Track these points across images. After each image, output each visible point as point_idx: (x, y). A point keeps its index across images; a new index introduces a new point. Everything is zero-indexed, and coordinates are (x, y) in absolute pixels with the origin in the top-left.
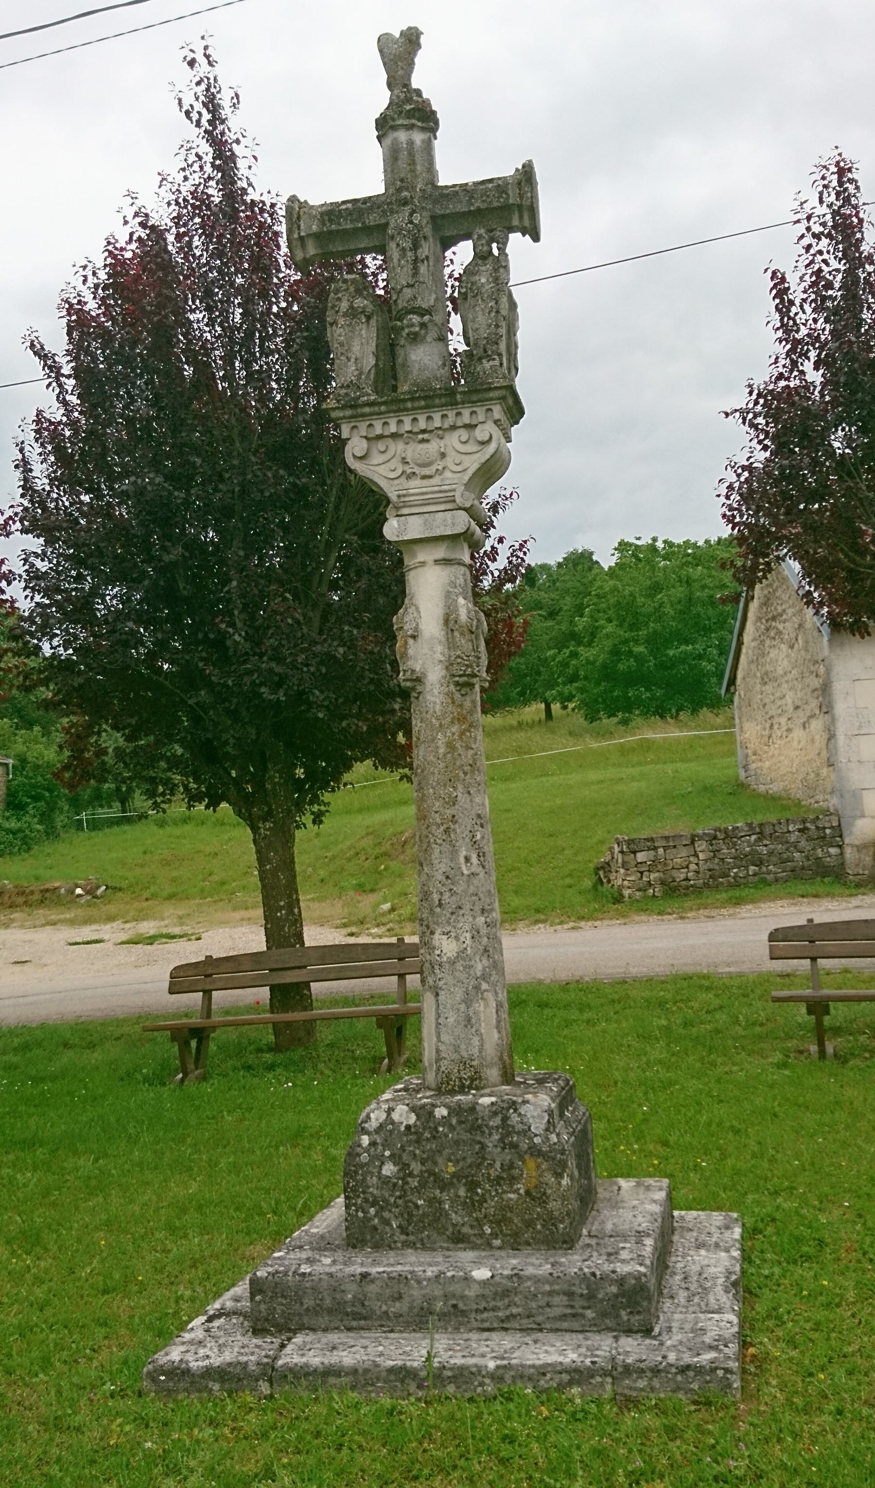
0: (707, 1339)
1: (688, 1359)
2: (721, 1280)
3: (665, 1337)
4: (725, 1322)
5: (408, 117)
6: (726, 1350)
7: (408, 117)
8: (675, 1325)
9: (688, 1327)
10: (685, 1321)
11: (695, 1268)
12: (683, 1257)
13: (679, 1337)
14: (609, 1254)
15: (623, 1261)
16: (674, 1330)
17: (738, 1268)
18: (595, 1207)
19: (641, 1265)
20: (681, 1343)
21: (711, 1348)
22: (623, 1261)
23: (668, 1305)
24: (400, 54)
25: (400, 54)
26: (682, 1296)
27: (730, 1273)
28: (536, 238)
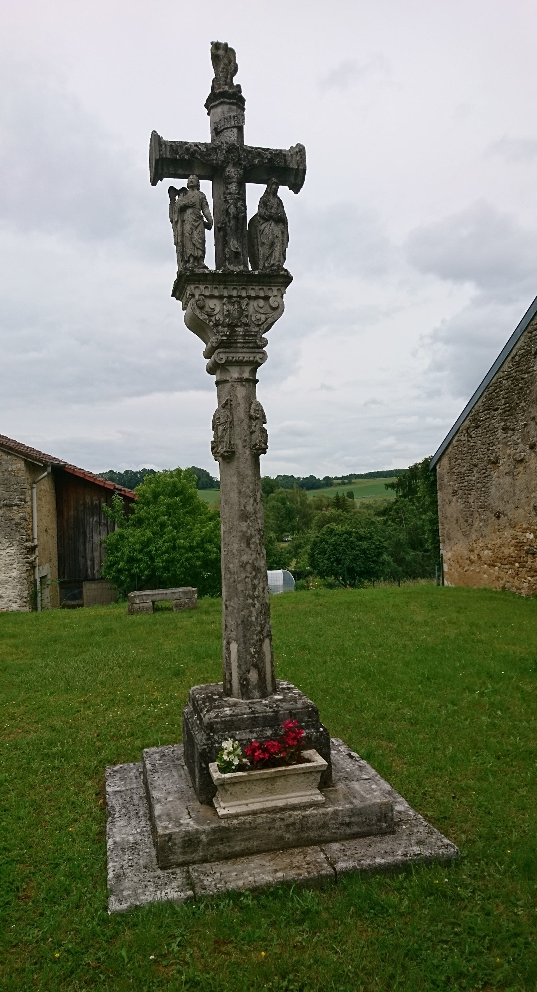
0: (118, 775)
1: (125, 765)
2: (117, 815)
3: (137, 773)
4: (112, 787)
5: (226, 98)
6: (110, 771)
7: (226, 98)
8: (135, 781)
9: (128, 781)
10: (131, 784)
11: (133, 822)
12: (143, 831)
13: (131, 774)
14: (164, 755)
15: (156, 753)
16: (134, 778)
17: (108, 826)
18: (192, 789)
19: (147, 752)
20: (130, 772)
21: (116, 771)
22: (156, 753)
23: (142, 793)
24: (223, 58)
25: (223, 58)
26: (136, 801)
27: (112, 822)
28: (156, 139)
